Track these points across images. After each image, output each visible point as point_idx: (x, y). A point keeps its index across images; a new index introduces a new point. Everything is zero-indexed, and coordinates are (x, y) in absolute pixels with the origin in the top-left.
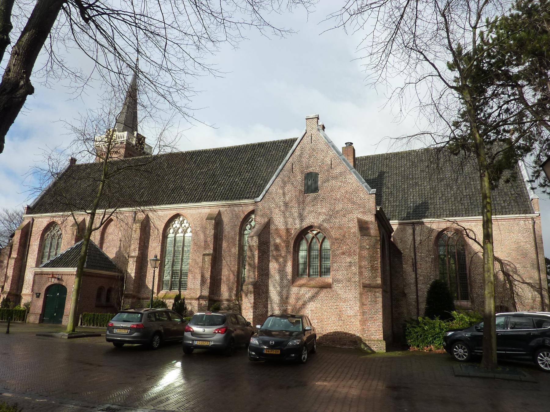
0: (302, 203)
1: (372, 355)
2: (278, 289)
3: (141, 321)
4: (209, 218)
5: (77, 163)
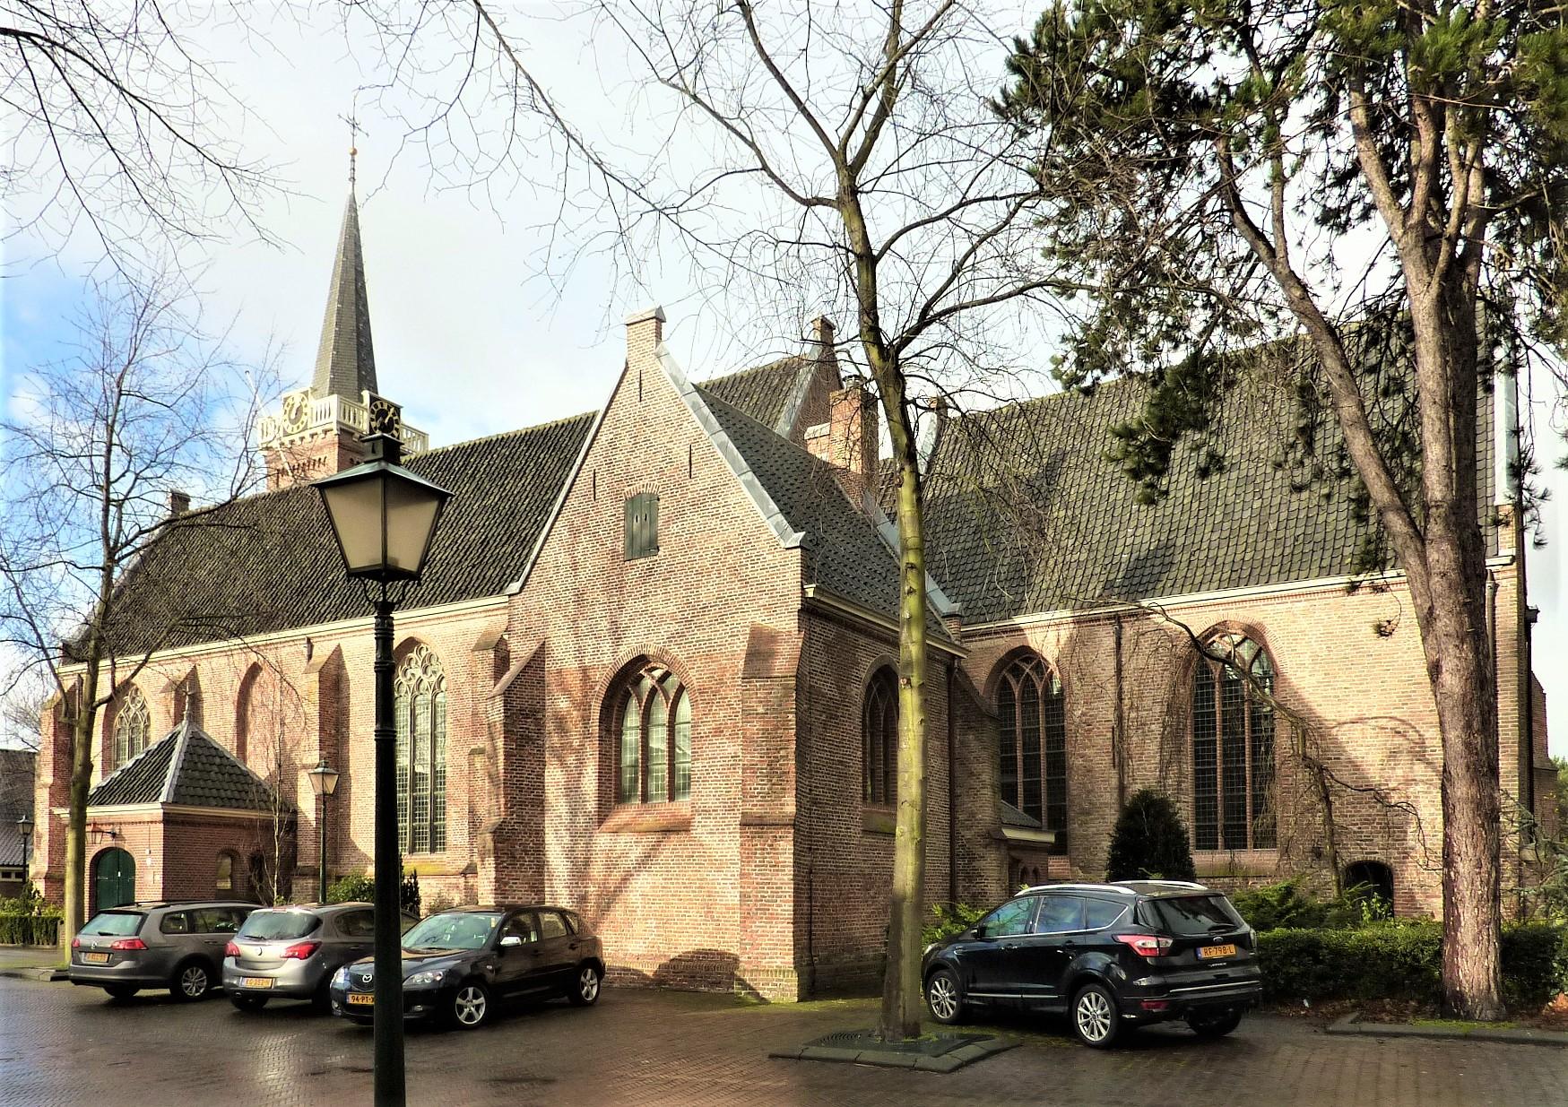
0: (616, 587)
1: (762, 1009)
2: (567, 840)
3: (137, 934)
4: (480, 647)
5: (194, 506)
